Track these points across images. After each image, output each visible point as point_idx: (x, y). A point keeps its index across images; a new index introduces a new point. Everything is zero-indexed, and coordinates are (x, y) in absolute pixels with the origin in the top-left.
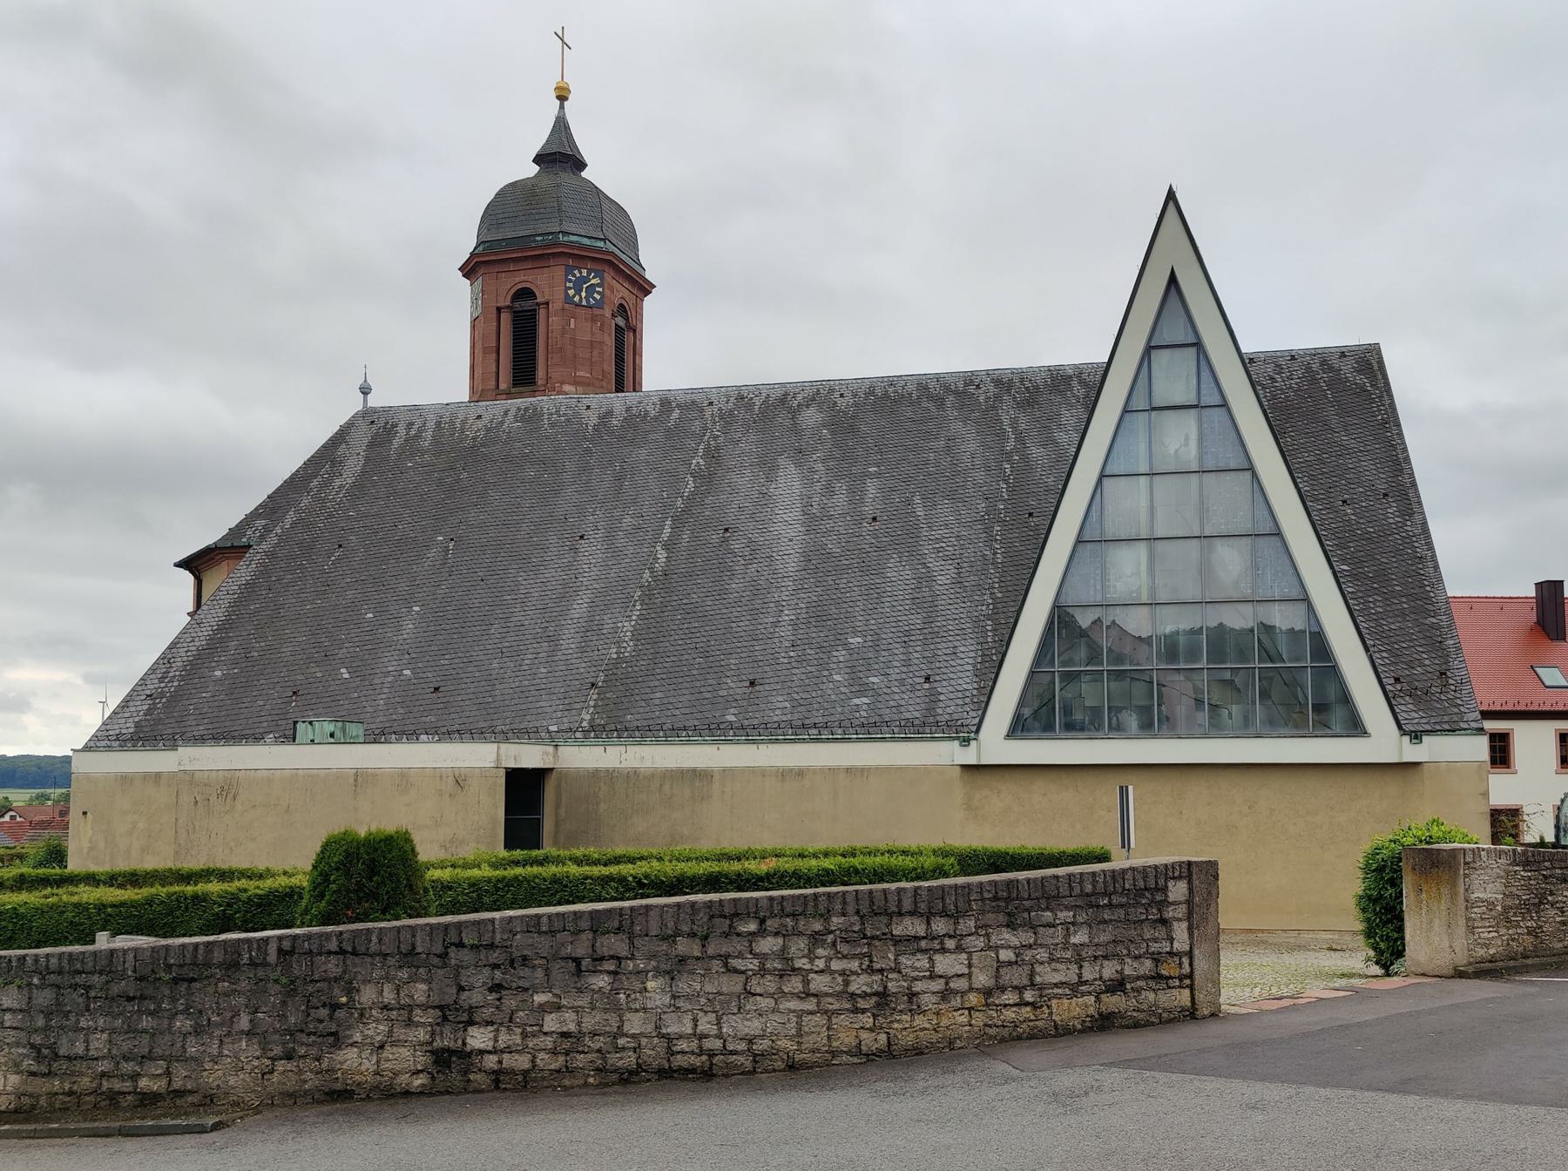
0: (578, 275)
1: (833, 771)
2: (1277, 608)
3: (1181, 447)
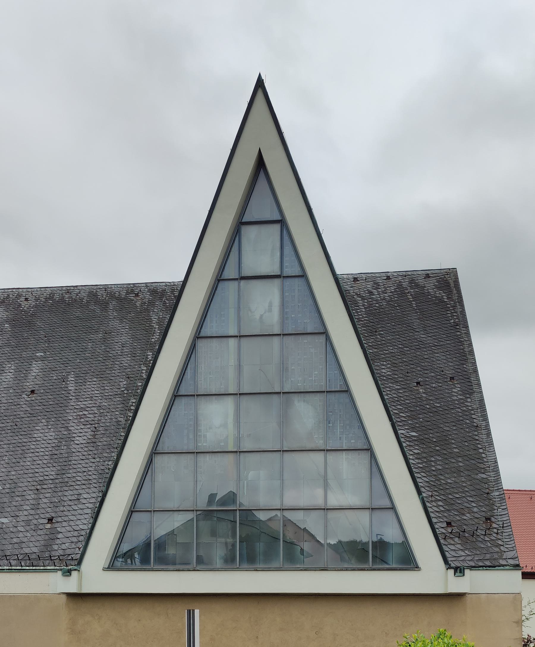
3: (265, 313)
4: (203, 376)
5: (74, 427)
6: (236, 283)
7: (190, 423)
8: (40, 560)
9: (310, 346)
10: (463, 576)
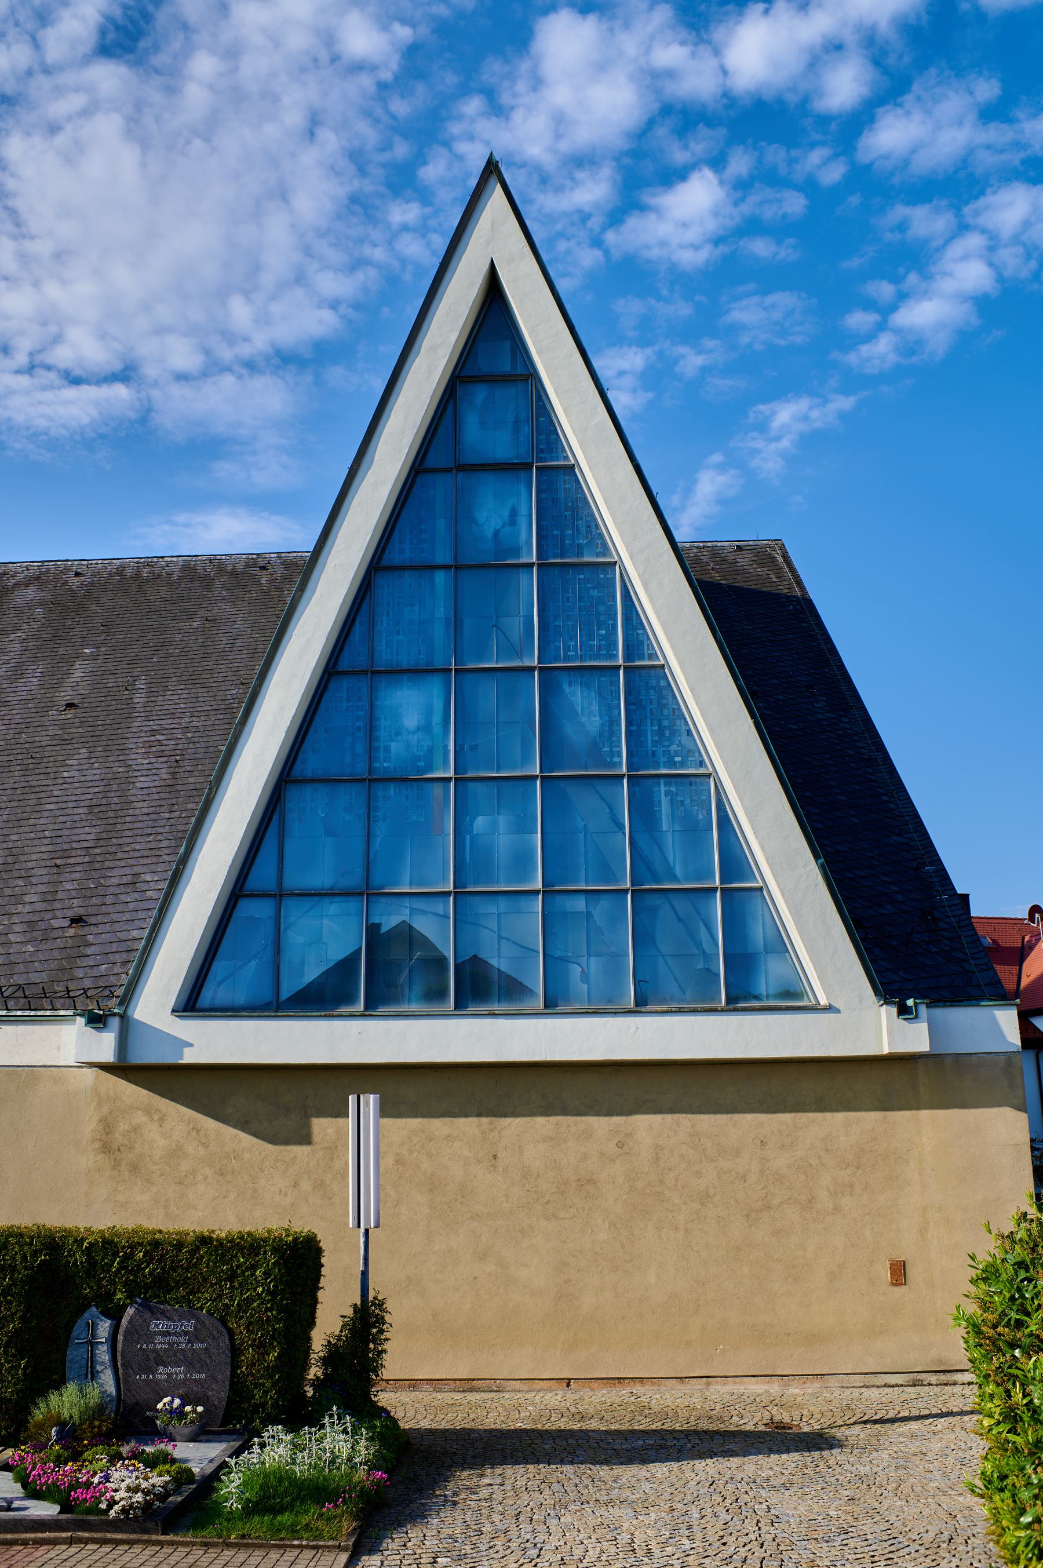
2: (663, 789)
3: (503, 526)
4: (384, 637)
5: (139, 759)
6: (449, 478)
7: (359, 724)
8: (46, 997)
9: (589, 586)
10: (915, 1018)
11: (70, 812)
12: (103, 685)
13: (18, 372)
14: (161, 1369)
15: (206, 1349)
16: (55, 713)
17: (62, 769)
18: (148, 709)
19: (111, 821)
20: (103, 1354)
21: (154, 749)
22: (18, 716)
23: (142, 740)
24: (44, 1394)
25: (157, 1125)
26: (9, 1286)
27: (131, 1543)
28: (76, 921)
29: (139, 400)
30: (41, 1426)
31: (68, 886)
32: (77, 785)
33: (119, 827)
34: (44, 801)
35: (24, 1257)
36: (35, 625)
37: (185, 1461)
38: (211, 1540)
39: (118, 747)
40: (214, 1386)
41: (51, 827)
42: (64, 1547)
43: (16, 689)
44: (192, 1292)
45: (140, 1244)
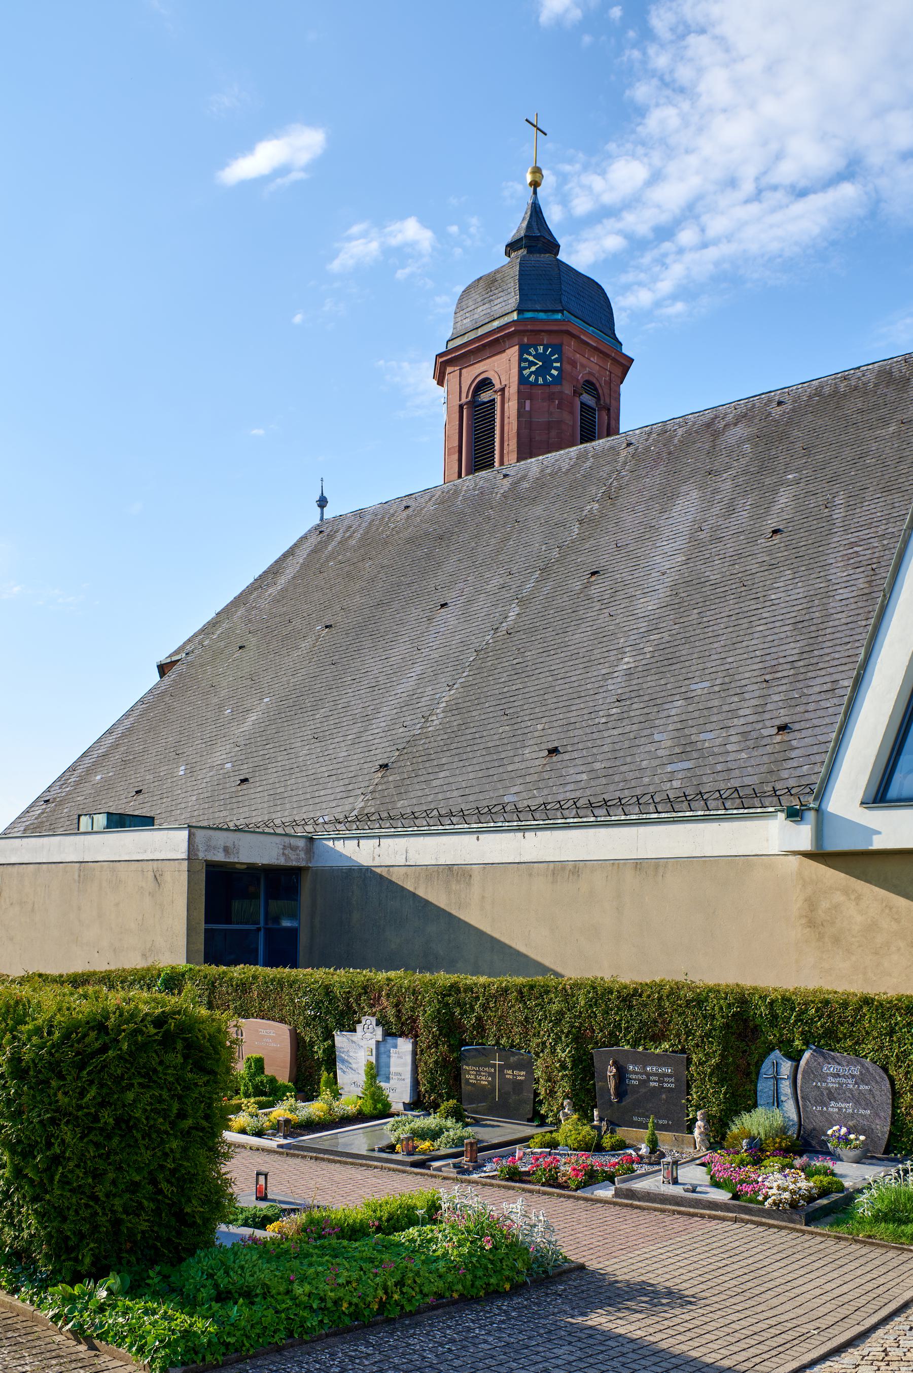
0: (555, 365)
1: (616, 863)
5: (838, 574)
11: (776, 630)
12: (805, 507)
13: (747, 201)
14: (833, 1103)
15: (870, 1090)
16: (763, 541)
17: (770, 592)
18: (846, 523)
19: (813, 635)
20: (786, 1088)
21: (852, 561)
22: (732, 550)
23: (841, 554)
24: (737, 1113)
25: (854, 903)
26: (710, 1030)
27: (781, 1228)
28: (782, 728)
29: (866, 193)
30: (736, 1138)
31: (776, 698)
32: (783, 605)
33: (820, 639)
34: (754, 624)
35: (721, 1008)
36: (743, 461)
37: (842, 1176)
38: (843, 1235)
39: (819, 564)
40: (877, 1121)
41: (761, 646)
42: (730, 1223)
43: (729, 525)
44: (856, 1043)
45: (813, 1002)
